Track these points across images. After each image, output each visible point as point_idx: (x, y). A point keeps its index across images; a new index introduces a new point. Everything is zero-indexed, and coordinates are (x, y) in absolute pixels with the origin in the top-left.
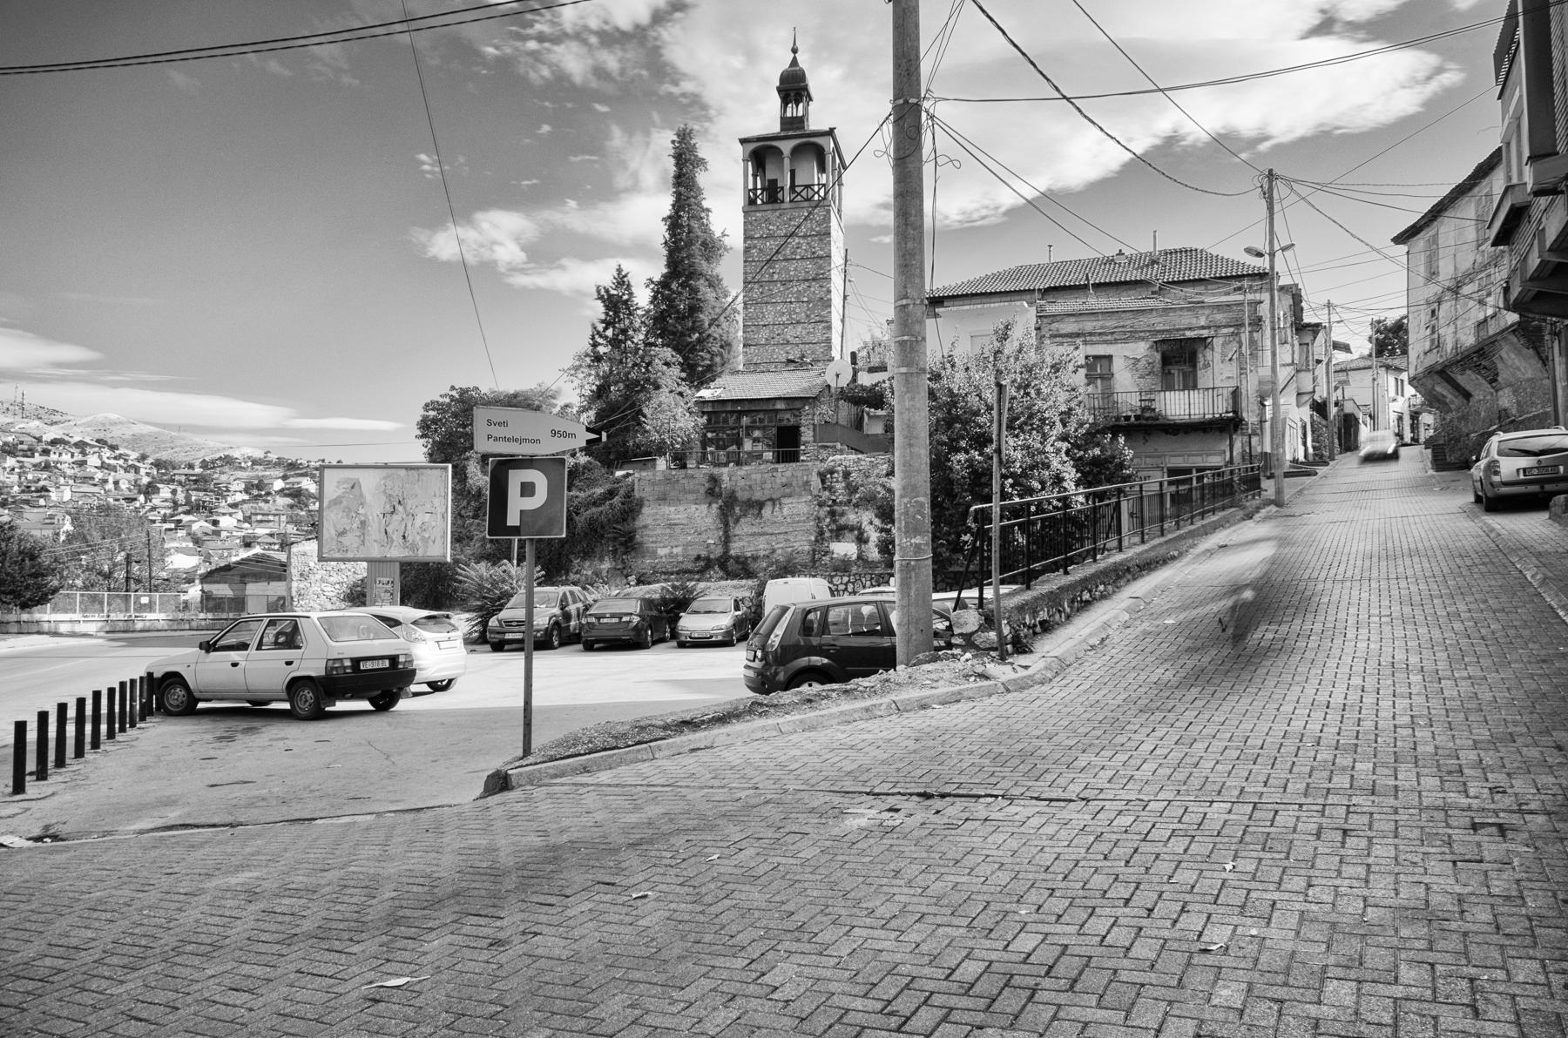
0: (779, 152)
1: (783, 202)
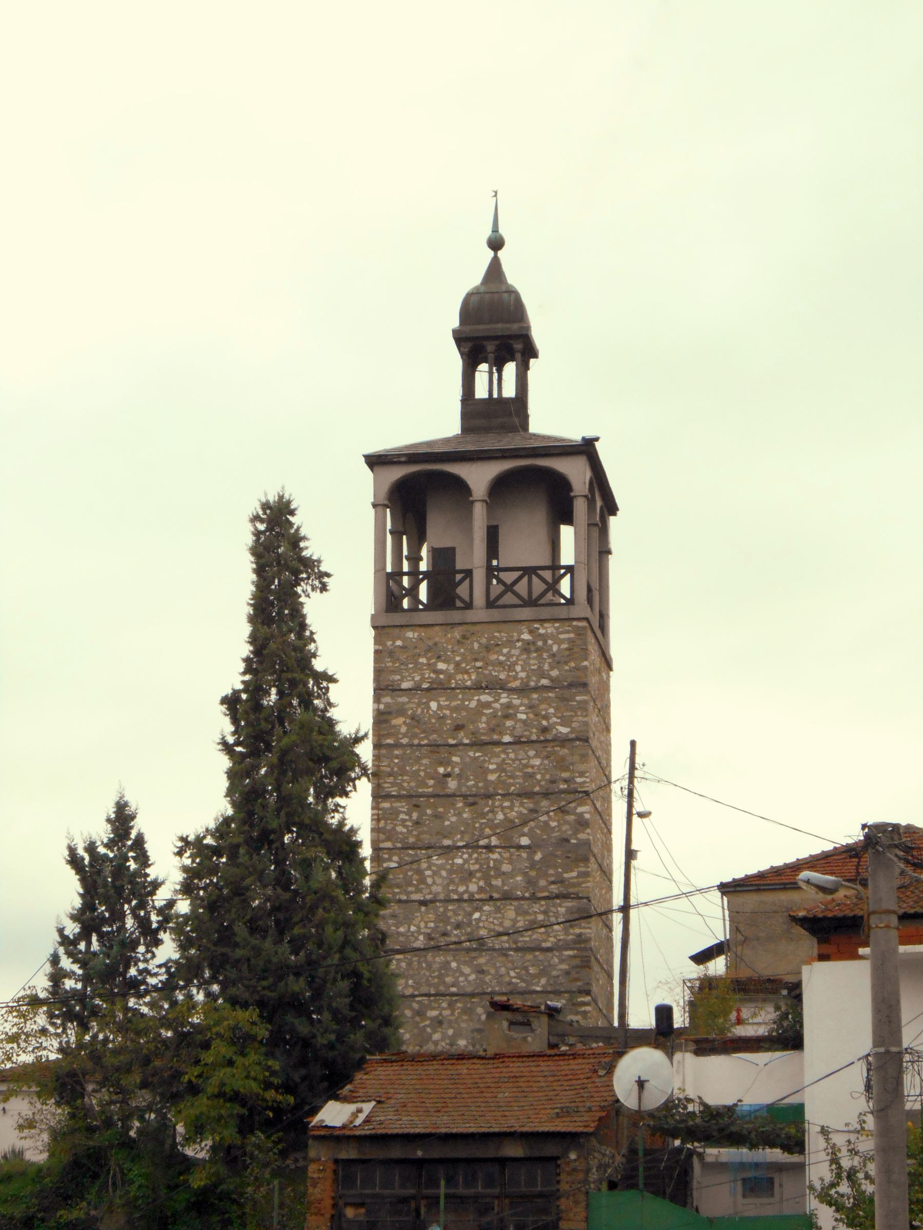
0: (460, 487)
1: (469, 606)
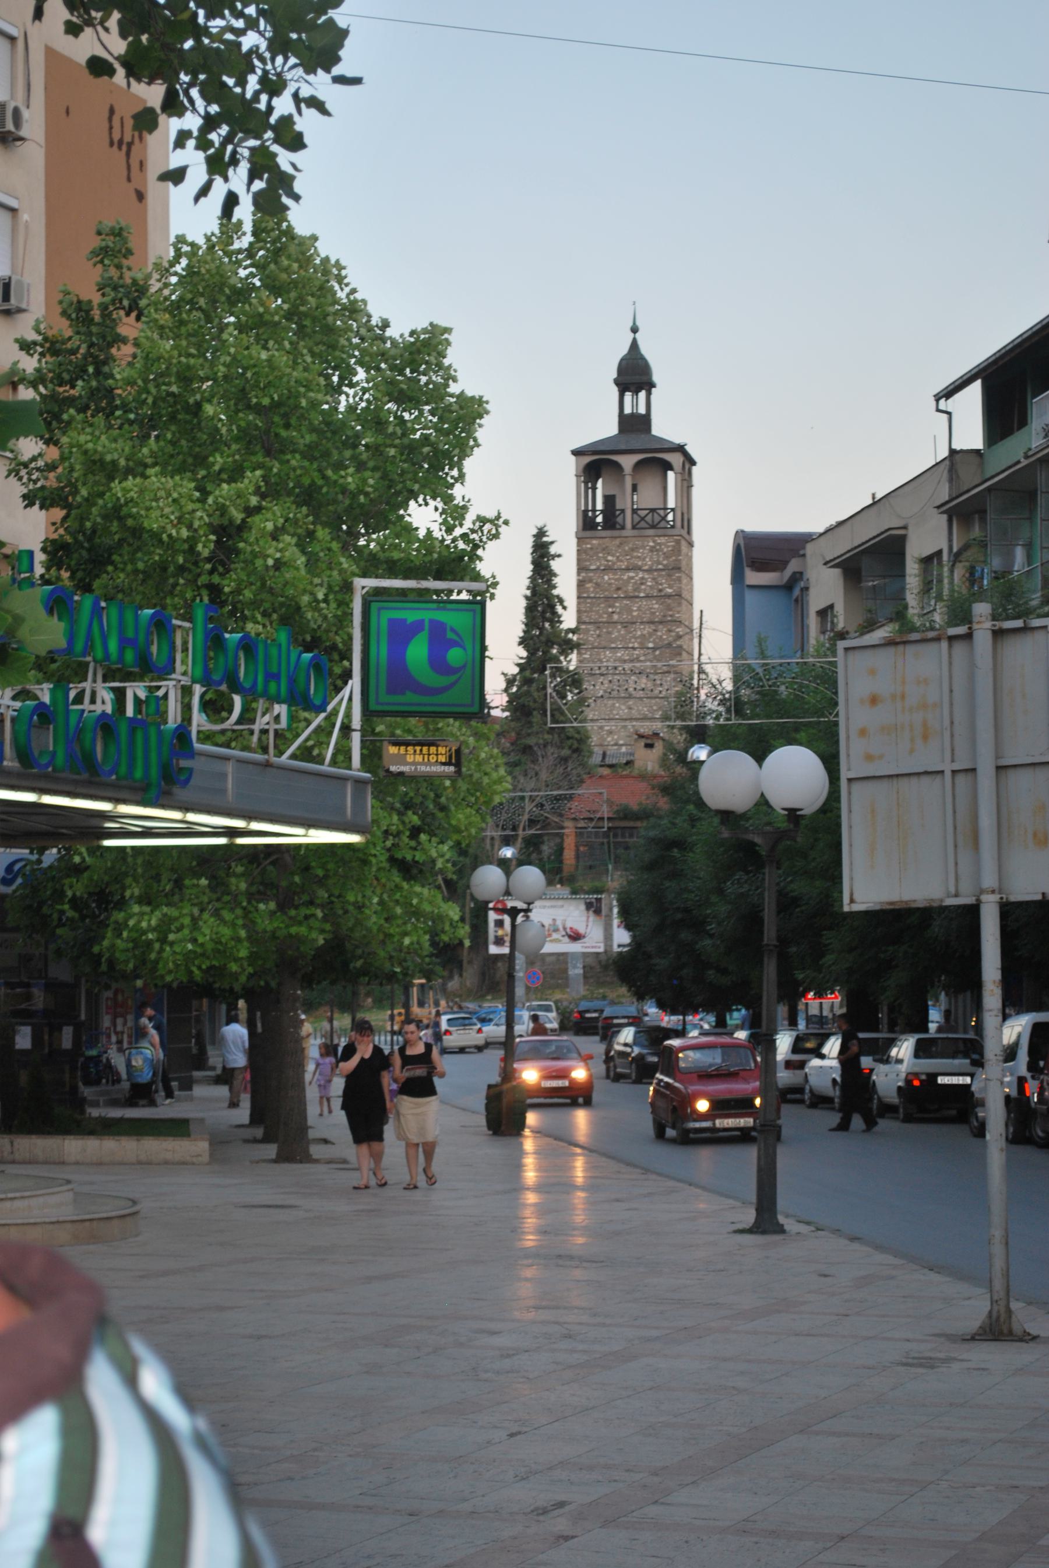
0: (617, 467)
1: (623, 528)
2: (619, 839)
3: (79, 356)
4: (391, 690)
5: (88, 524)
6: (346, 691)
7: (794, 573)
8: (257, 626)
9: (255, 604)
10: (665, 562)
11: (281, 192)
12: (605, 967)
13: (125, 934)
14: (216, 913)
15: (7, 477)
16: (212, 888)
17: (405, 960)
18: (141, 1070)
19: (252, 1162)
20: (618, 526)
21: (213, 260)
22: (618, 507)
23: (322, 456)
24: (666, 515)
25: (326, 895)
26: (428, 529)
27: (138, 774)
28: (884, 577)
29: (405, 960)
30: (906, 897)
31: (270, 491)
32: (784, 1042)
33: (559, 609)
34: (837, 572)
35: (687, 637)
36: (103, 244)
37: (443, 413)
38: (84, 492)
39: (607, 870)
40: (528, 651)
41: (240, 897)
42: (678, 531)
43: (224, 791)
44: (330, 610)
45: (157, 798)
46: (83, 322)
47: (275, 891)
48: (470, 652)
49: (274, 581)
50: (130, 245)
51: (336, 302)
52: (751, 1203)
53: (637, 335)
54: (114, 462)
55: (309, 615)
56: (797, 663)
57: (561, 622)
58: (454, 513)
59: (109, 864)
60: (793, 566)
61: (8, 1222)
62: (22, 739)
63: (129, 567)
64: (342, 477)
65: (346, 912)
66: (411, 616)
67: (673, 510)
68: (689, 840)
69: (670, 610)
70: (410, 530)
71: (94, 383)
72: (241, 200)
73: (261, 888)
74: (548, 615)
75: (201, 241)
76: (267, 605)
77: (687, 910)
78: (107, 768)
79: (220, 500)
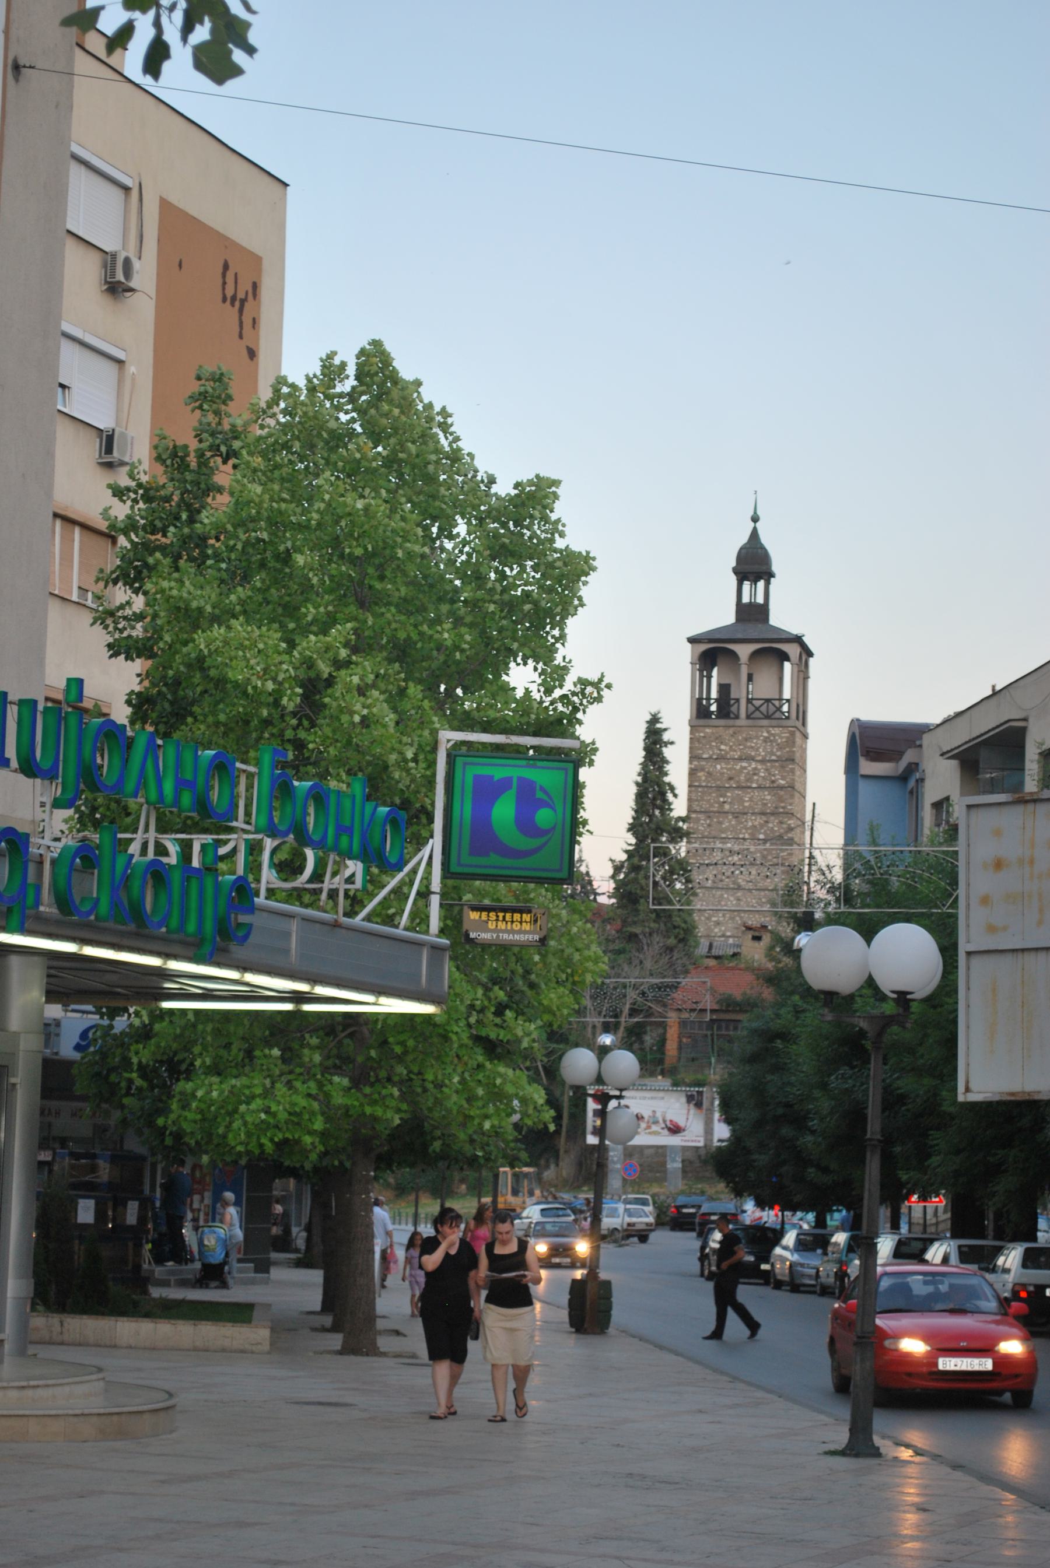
0: (733, 655)
1: (737, 717)
2: (724, 1032)
3: (173, 504)
4: (475, 851)
5: (171, 673)
6: (426, 852)
7: (910, 764)
8: (341, 785)
9: (340, 761)
10: (779, 753)
11: (231, 46)
12: (705, 1162)
13: (194, 1105)
14: (289, 1084)
15: (92, 625)
16: (284, 1060)
17: (488, 1145)
18: (214, 1250)
19: (315, 1353)
20: (732, 716)
21: (314, 405)
22: (733, 696)
23: (417, 611)
24: (781, 706)
25: (405, 1072)
26: (527, 689)
27: (191, 927)
28: (1003, 769)
29: (488, 1145)
30: (1030, 1087)
31: (359, 646)
32: (885, 1246)
33: (670, 796)
34: (954, 763)
35: (798, 830)
36: (202, 389)
37: (546, 568)
38: (167, 638)
39: (710, 1063)
40: (636, 838)
41: (313, 1070)
42: (792, 722)
43: (287, 951)
44: (418, 771)
45: (211, 954)
46: (178, 469)
47: (351, 1066)
48: (560, 810)
49: (362, 739)
50: (230, 391)
51: (438, 450)
52: (845, 1421)
53: (758, 525)
54: (200, 610)
55: (397, 775)
56: (910, 852)
57: (671, 810)
58: (554, 676)
59: (178, 1031)
60: (909, 757)
61: (27, 1412)
62: (62, 882)
63: (210, 719)
64: (438, 632)
65: (425, 1090)
66: (498, 772)
67: (788, 701)
68: (793, 1032)
69: (782, 802)
70: (507, 689)
71: (186, 530)
72: (173, 51)
73: (337, 1062)
74: (658, 802)
75: (302, 383)
76: (352, 763)
77: (788, 1105)
78: (156, 919)
79: (308, 653)
